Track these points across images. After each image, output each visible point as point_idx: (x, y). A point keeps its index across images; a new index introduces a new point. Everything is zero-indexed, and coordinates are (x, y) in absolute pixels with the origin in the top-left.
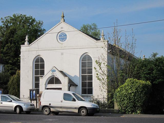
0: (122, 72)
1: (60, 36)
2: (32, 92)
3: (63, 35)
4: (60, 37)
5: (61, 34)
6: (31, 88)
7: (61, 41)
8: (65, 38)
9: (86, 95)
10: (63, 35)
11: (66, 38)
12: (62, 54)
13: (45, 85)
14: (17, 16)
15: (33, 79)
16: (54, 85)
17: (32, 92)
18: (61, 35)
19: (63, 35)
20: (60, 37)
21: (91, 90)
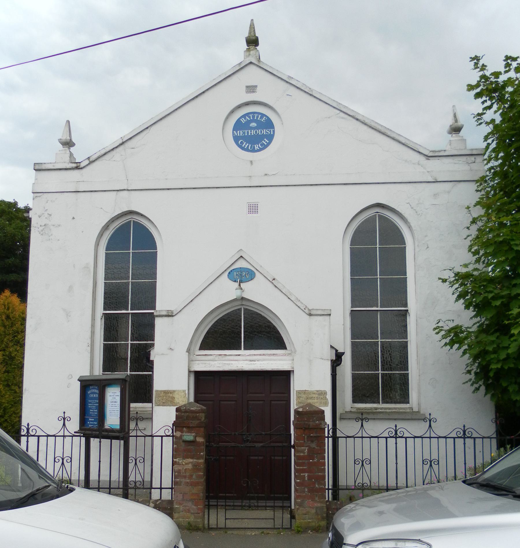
0: (137, 366)
1: (238, 126)
2: (93, 393)
3: (253, 124)
4: (240, 133)
5: (244, 116)
6: (86, 373)
7: (247, 150)
8: (263, 137)
9: (375, 405)
10: (253, 124)
11: (270, 138)
12: (253, 209)
13: (188, 351)
14: (11, 427)
15: (93, 326)
16: (242, 352)
17: (93, 393)
18: (243, 121)
19: (252, 121)
20: (240, 133)
21: (404, 381)
